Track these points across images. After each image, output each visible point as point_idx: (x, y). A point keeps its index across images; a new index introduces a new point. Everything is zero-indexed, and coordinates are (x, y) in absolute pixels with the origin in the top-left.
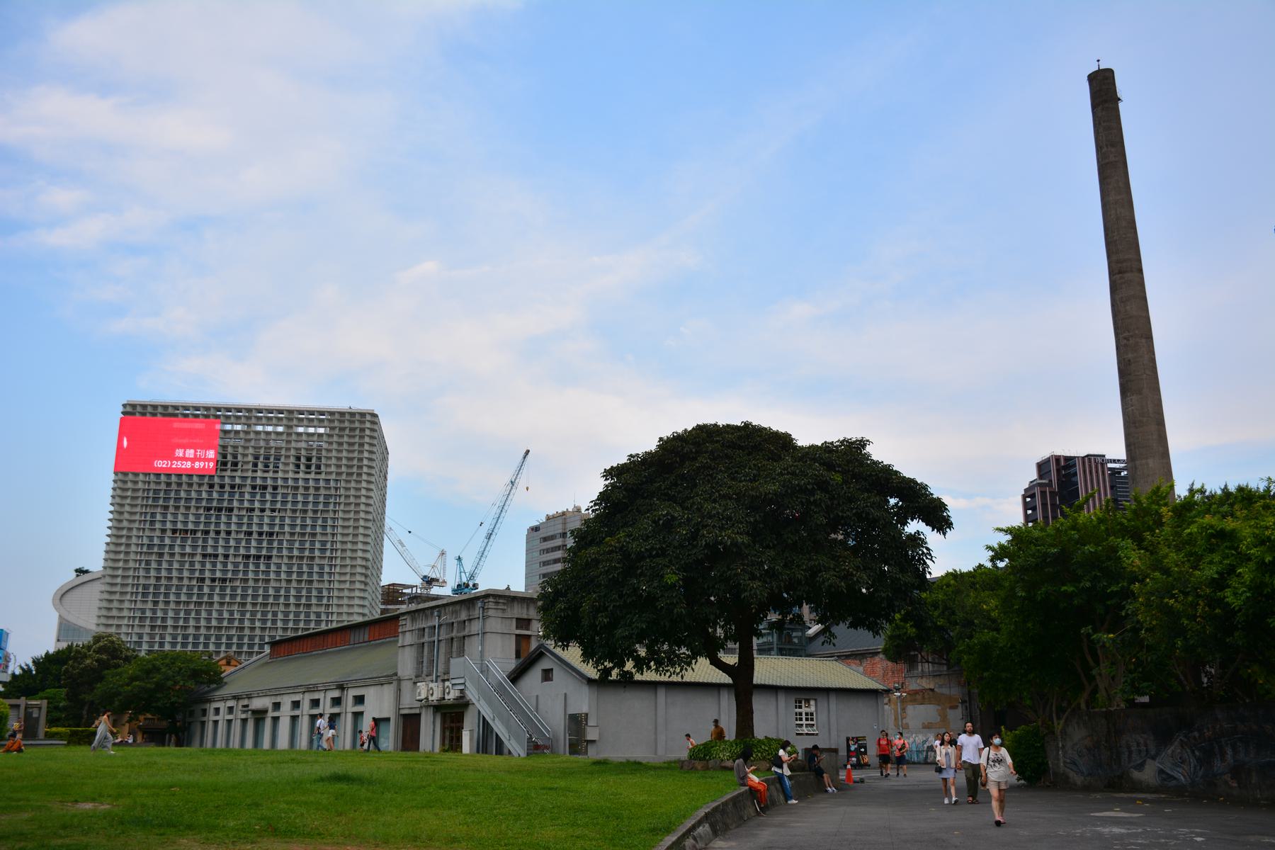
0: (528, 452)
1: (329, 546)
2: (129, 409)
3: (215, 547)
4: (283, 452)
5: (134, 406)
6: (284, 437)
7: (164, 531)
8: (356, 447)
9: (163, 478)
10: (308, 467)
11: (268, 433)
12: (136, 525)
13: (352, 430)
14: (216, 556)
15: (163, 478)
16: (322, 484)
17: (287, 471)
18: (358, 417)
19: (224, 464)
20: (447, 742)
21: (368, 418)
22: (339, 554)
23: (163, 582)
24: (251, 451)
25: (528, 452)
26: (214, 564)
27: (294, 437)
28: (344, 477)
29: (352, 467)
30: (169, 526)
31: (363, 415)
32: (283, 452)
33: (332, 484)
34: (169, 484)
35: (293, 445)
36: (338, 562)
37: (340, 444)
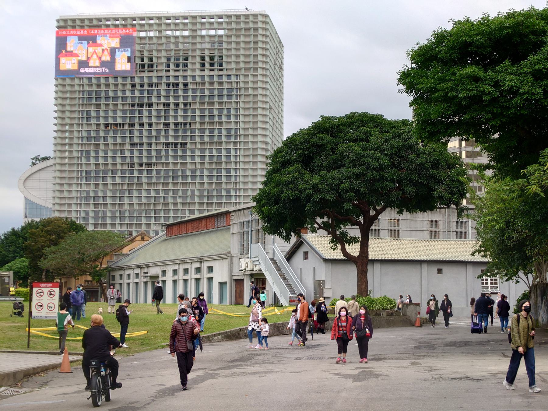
2: (62, 24)
3: (141, 137)
5: (65, 21)
7: (98, 125)
10: (212, 65)
23: (101, 168)
26: (140, 152)
32: (190, 53)
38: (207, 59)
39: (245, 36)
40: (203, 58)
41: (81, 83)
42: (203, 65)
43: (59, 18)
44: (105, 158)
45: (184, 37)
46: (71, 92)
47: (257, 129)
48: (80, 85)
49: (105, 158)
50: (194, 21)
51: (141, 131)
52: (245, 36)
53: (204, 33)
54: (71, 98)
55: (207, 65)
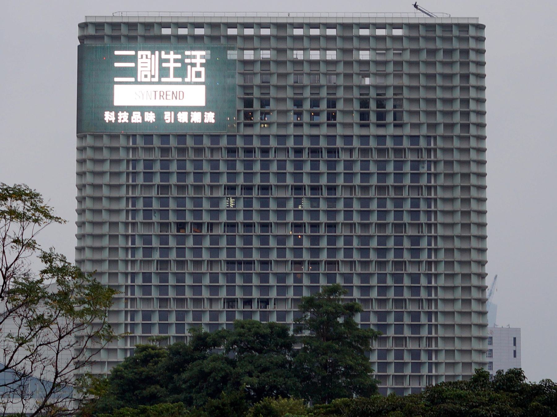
0: (496, 276)
1: (424, 244)
2: (91, 31)
3: (247, 251)
4: (340, 93)
5: (99, 26)
6: (340, 68)
7: (164, 226)
8: (457, 81)
9: (156, 143)
10: (381, 116)
11: (313, 63)
12: (122, 218)
13: (449, 52)
14: (250, 263)
15: (156, 143)
16: (406, 144)
17: (347, 124)
18: (456, 32)
19: (248, 116)
20: (133, 28)
21: (472, 32)
22: (441, 256)
23: (173, 306)
24: (290, 93)
25: (496, 276)
26: (248, 278)
27: (356, 68)
28: (441, 131)
29: (451, 113)
30: (172, 218)
31: (464, 27)
32: (340, 93)
33: (423, 144)
34: (165, 151)
35: (356, 80)
36: (441, 269)
37: (432, 52)
38: (373, 105)
39: (111, 186)
40: (364, 103)
41: (131, 144)
42: (364, 116)
43: (83, 21)
44: (180, 289)
45: (328, 63)
46: (112, 161)
47: (470, 313)
48: (127, 149)
49: (180, 289)
51: (248, 240)
52: (111, 186)
53: (299, 55)
54: (112, 174)
55: (373, 118)
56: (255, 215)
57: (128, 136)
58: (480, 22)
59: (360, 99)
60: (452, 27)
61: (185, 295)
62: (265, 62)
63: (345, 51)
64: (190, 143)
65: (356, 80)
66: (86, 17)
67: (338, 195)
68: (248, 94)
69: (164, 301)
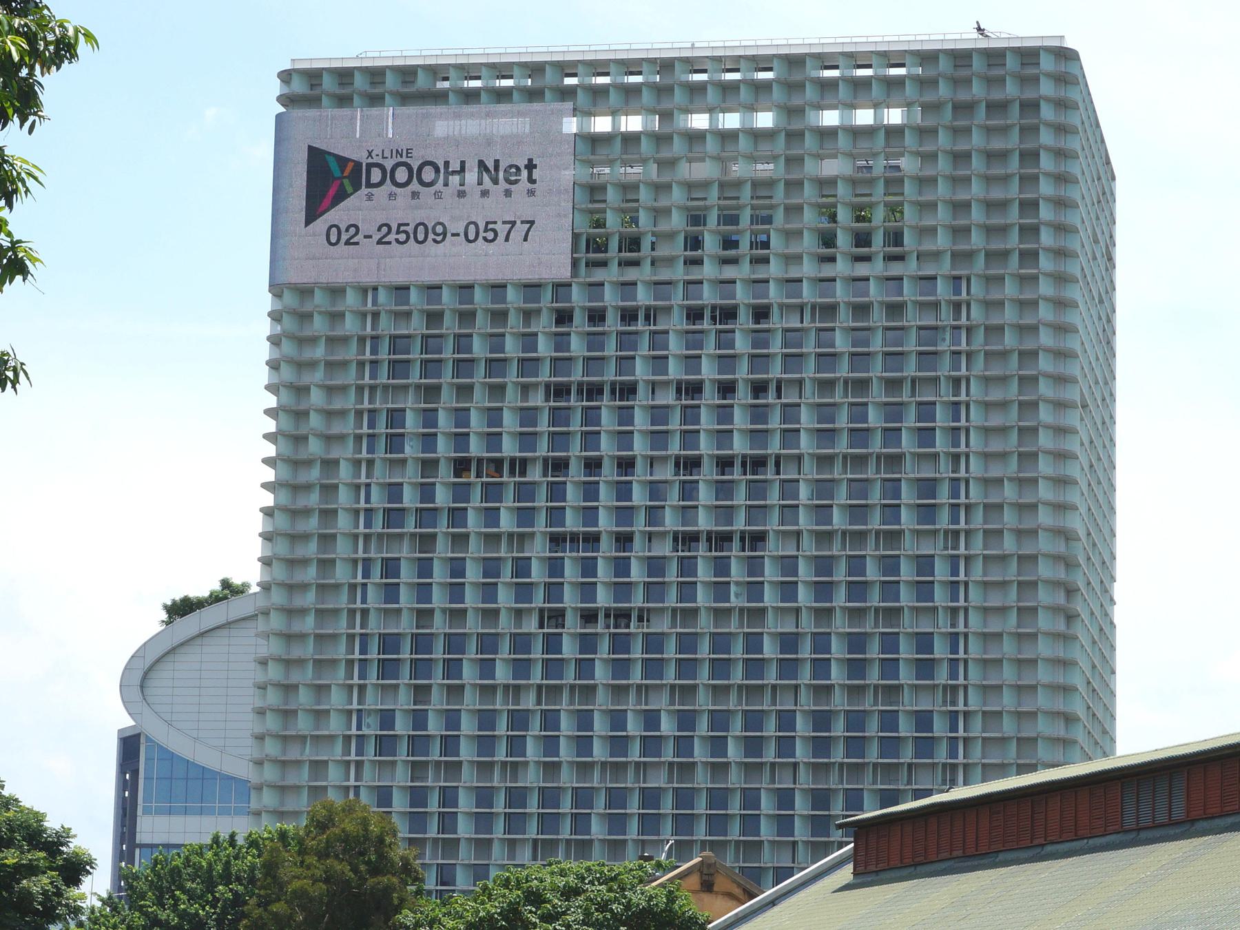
2: (298, 87)
3: (590, 514)
5: (313, 76)
10: (862, 239)
16: (909, 292)
21: (1047, 63)
26: (589, 567)
44: (456, 592)
50: (796, 77)
56: (804, 439)
57: (364, 290)
58: (1069, 44)
59: (687, 209)
60: (971, 57)
61: (898, 601)
62: (894, 133)
63: (666, 116)
64: (513, 297)
65: (811, 168)
66: (293, 60)
67: (838, 399)
68: (628, 201)
69: (824, 614)
